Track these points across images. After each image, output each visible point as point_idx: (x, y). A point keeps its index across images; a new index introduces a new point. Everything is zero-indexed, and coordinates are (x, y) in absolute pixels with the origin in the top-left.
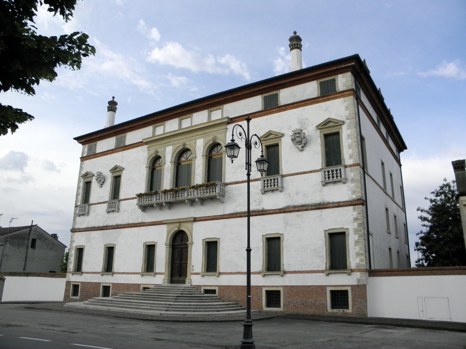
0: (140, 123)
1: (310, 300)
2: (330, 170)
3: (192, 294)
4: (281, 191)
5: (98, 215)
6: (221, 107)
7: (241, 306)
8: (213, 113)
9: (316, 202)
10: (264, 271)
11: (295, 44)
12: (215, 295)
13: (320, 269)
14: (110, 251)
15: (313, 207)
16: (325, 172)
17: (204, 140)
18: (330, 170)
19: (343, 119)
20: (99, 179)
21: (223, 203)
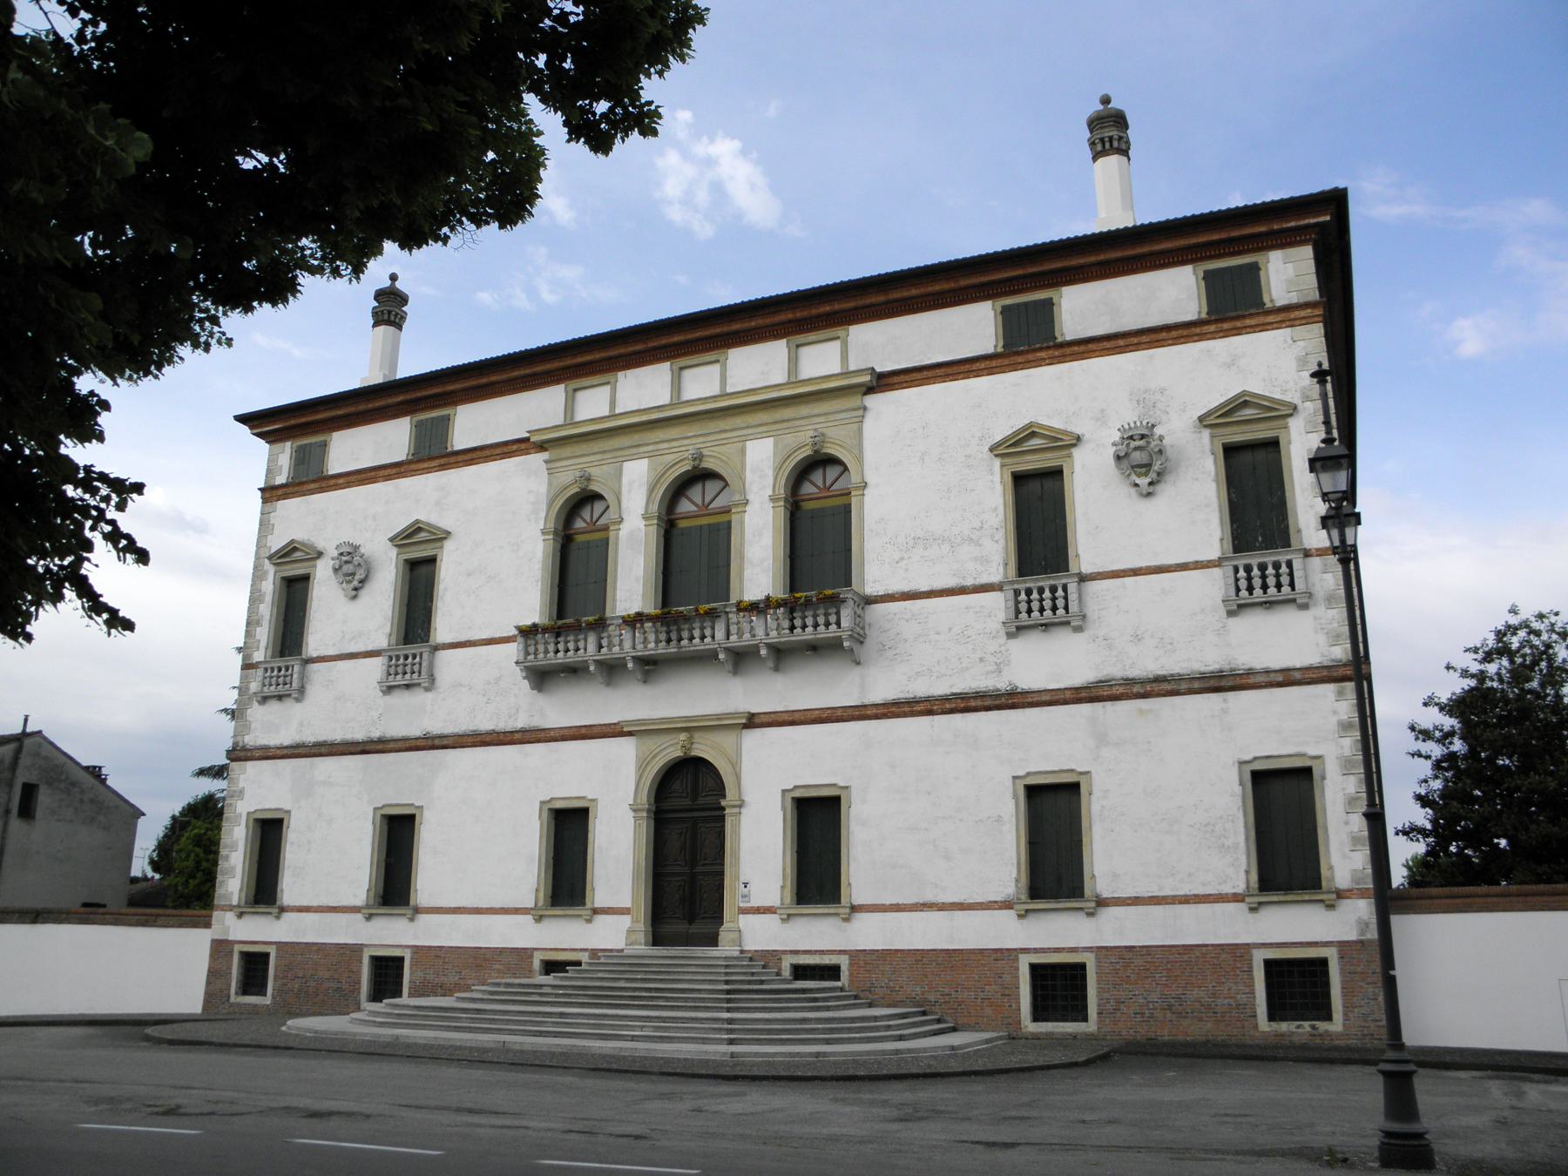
0: (516, 373)
1: (1196, 993)
2: (1254, 562)
3: (762, 982)
4: (1079, 629)
5: (345, 697)
6: (840, 332)
7: (939, 1021)
8: (581, 395)
9: (1203, 669)
10: (1024, 897)
11: (1111, 138)
12: (839, 984)
13: (1228, 889)
14: (398, 835)
15: (1196, 685)
16: (1236, 570)
17: (776, 444)
18: (1254, 562)
19: (1292, 397)
20: (346, 568)
21: (858, 663)
